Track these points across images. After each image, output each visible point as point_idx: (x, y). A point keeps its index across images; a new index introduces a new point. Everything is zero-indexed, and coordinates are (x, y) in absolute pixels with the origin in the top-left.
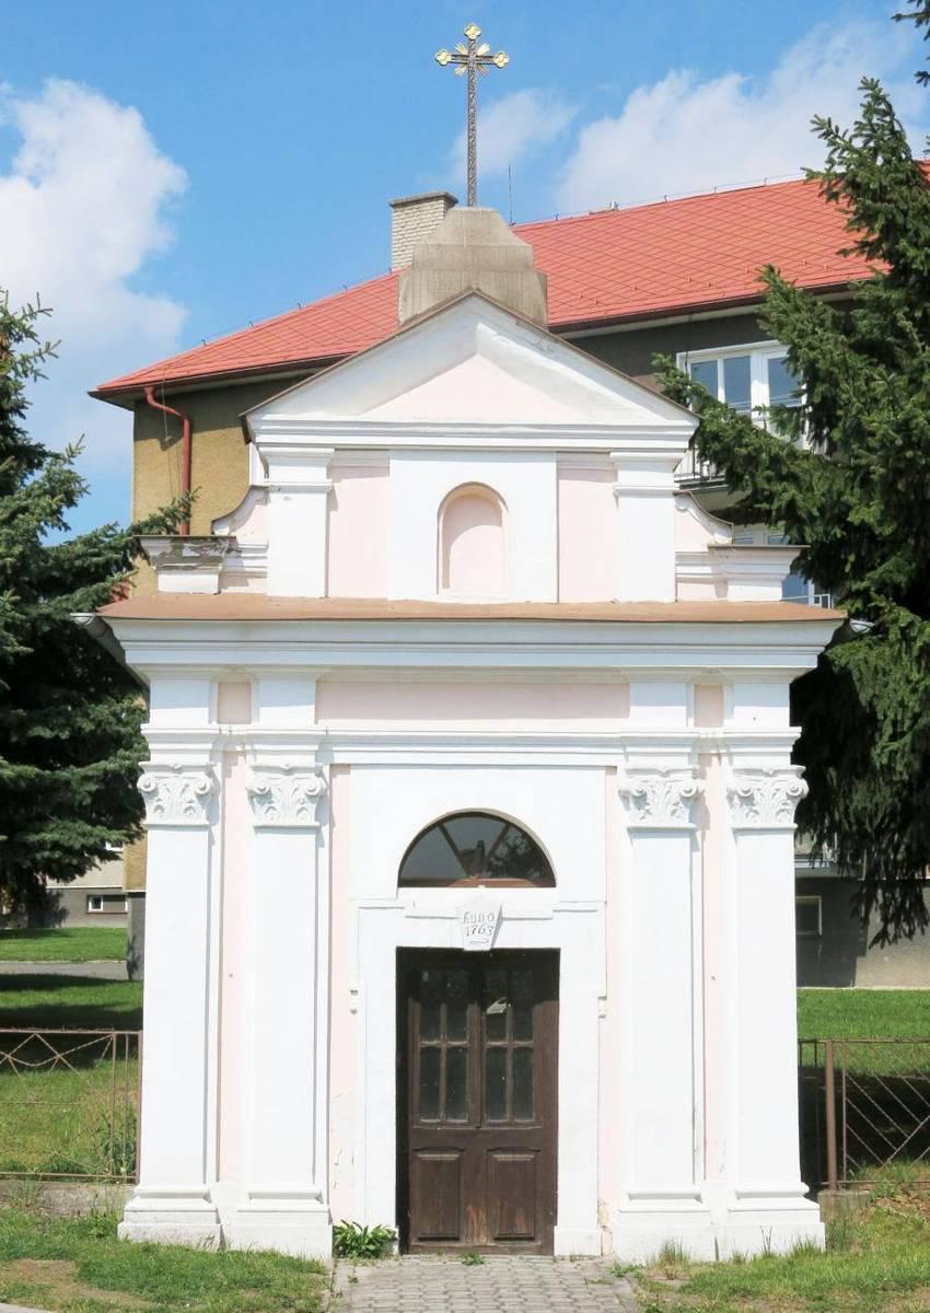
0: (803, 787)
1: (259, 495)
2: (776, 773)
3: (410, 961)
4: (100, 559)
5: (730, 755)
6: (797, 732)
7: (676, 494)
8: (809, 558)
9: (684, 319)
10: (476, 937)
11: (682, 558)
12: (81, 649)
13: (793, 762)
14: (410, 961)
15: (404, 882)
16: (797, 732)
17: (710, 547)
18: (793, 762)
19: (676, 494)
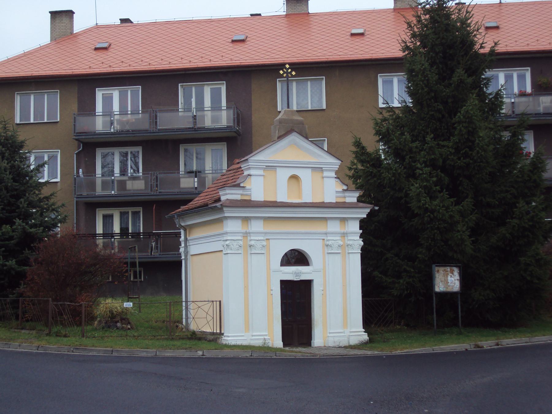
0: (362, 243)
1: (249, 177)
2: (357, 240)
3: (283, 282)
4: (21, 269)
5: (347, 236)
6: (361, 231)
7: (335, 178)
8: (363, 200)
9: (184, 72)
10: (297, 277)
11: (337, 192)
12: (410, 85)
13: (360, 238)
14: (283, 282)
15: (282, 264)
16: (361, 231)
17: (252, 15)
18: (360, 238)
19: (335, 178)
